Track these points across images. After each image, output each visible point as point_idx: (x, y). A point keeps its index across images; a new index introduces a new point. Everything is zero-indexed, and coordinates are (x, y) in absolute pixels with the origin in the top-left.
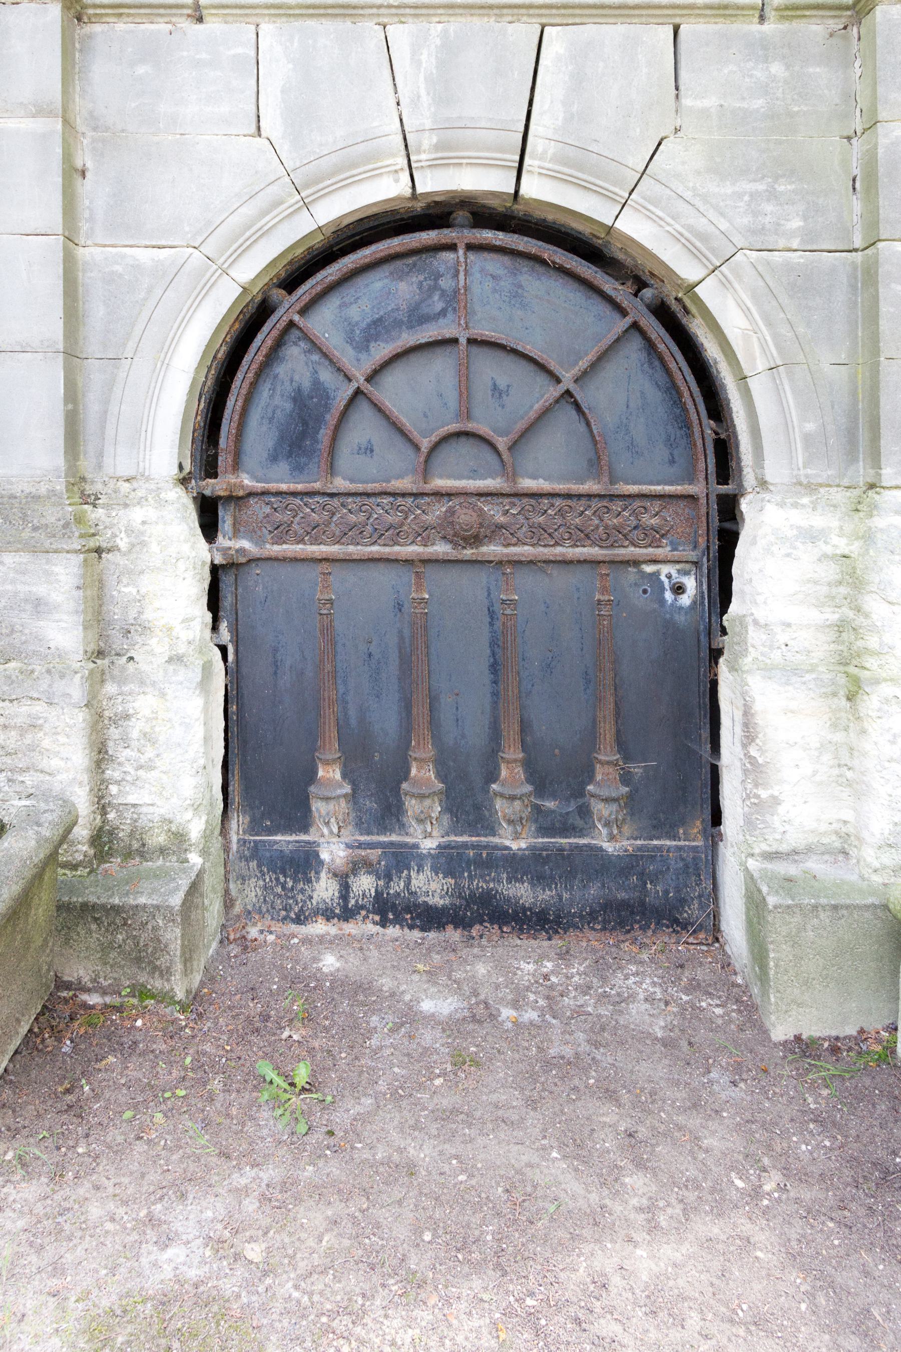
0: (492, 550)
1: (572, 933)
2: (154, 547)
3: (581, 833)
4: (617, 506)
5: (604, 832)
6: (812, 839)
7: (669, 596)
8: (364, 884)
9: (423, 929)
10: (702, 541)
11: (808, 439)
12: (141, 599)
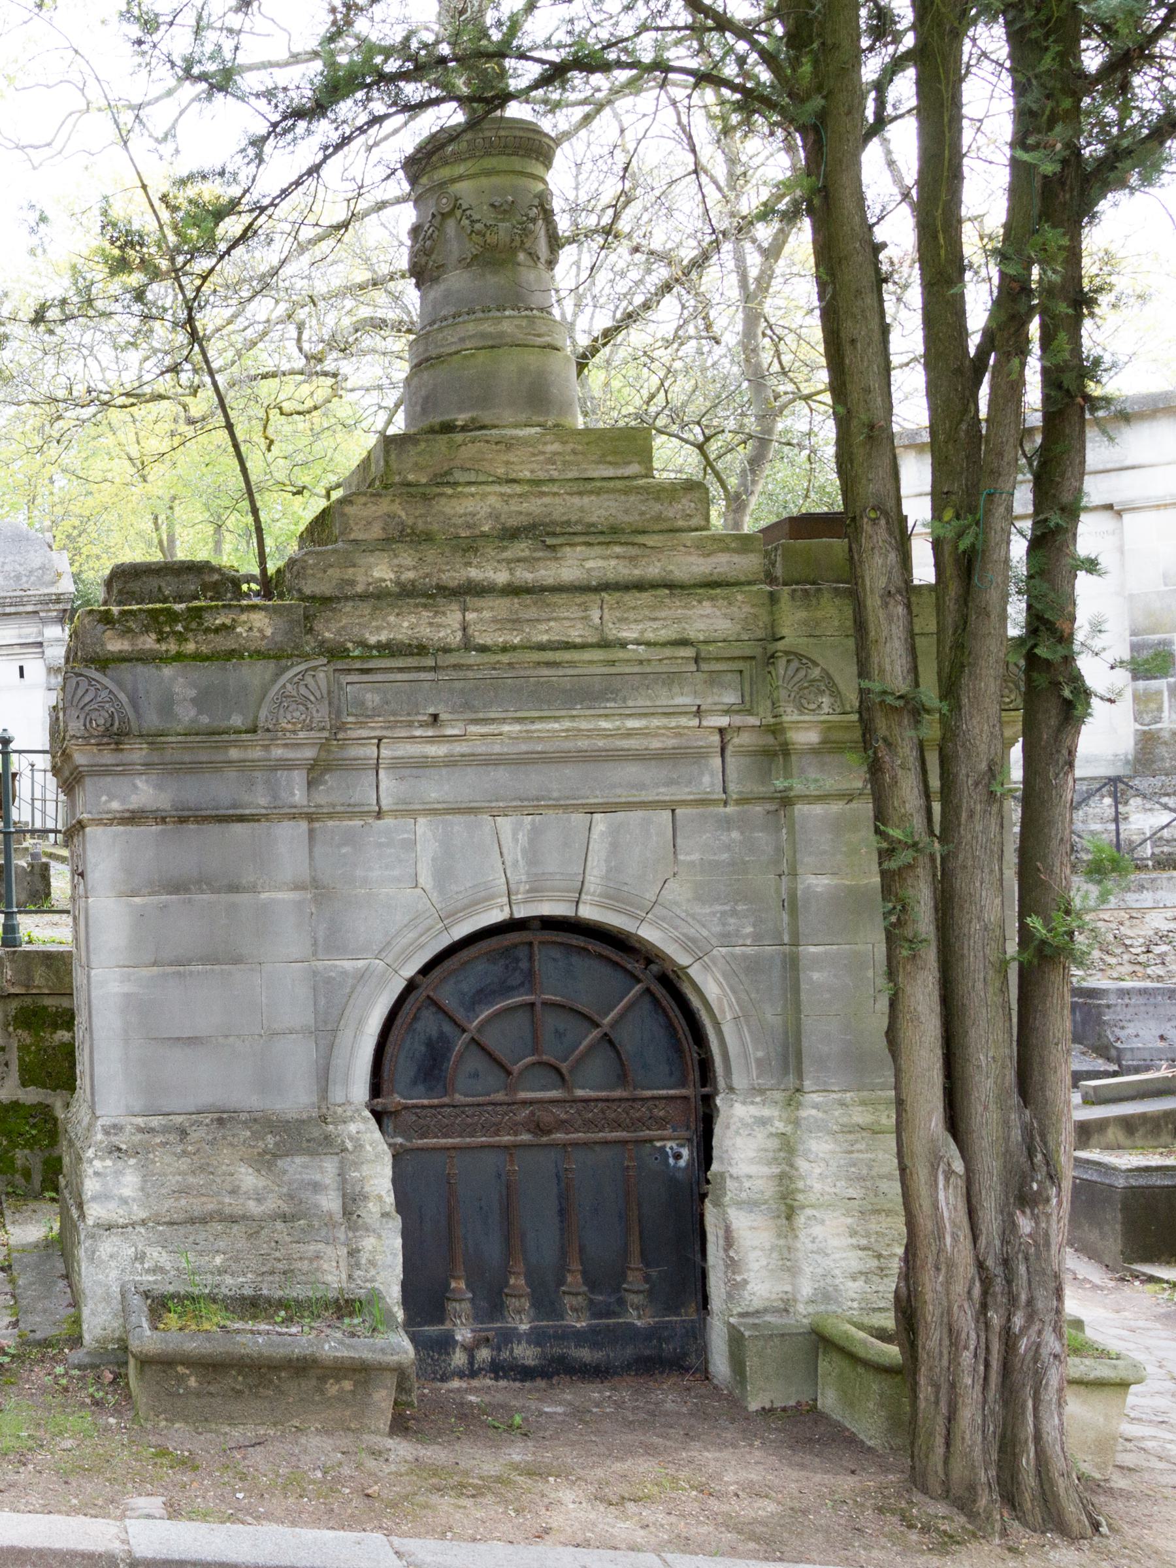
0: (559, 1136)
1: (616, 1378)
2: (368, 1148)
3: (615, 1314)
4: (637, 1105)
5: (635, 1313)
6: (767, 1304)
7: (671, 1161)
8: (484, 1354)
9: (522, 1381)
10: (693, 1127)
11: (759, 1062)
12: (362, 1180)
